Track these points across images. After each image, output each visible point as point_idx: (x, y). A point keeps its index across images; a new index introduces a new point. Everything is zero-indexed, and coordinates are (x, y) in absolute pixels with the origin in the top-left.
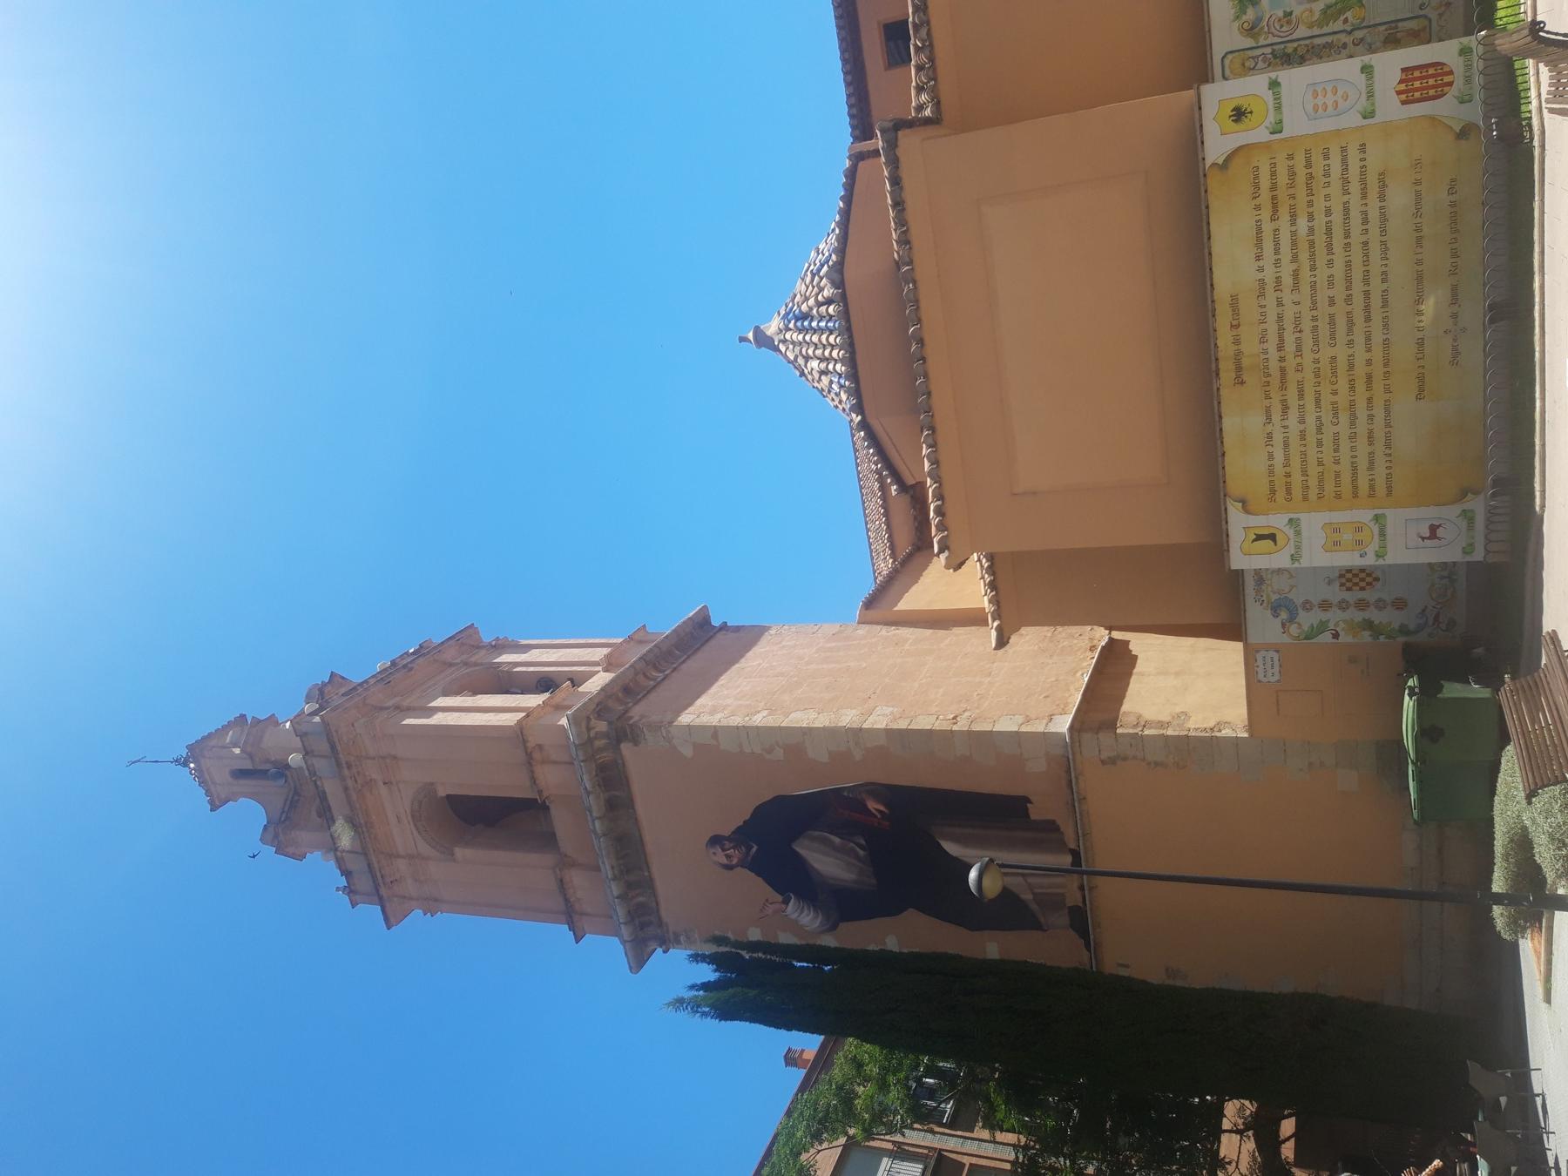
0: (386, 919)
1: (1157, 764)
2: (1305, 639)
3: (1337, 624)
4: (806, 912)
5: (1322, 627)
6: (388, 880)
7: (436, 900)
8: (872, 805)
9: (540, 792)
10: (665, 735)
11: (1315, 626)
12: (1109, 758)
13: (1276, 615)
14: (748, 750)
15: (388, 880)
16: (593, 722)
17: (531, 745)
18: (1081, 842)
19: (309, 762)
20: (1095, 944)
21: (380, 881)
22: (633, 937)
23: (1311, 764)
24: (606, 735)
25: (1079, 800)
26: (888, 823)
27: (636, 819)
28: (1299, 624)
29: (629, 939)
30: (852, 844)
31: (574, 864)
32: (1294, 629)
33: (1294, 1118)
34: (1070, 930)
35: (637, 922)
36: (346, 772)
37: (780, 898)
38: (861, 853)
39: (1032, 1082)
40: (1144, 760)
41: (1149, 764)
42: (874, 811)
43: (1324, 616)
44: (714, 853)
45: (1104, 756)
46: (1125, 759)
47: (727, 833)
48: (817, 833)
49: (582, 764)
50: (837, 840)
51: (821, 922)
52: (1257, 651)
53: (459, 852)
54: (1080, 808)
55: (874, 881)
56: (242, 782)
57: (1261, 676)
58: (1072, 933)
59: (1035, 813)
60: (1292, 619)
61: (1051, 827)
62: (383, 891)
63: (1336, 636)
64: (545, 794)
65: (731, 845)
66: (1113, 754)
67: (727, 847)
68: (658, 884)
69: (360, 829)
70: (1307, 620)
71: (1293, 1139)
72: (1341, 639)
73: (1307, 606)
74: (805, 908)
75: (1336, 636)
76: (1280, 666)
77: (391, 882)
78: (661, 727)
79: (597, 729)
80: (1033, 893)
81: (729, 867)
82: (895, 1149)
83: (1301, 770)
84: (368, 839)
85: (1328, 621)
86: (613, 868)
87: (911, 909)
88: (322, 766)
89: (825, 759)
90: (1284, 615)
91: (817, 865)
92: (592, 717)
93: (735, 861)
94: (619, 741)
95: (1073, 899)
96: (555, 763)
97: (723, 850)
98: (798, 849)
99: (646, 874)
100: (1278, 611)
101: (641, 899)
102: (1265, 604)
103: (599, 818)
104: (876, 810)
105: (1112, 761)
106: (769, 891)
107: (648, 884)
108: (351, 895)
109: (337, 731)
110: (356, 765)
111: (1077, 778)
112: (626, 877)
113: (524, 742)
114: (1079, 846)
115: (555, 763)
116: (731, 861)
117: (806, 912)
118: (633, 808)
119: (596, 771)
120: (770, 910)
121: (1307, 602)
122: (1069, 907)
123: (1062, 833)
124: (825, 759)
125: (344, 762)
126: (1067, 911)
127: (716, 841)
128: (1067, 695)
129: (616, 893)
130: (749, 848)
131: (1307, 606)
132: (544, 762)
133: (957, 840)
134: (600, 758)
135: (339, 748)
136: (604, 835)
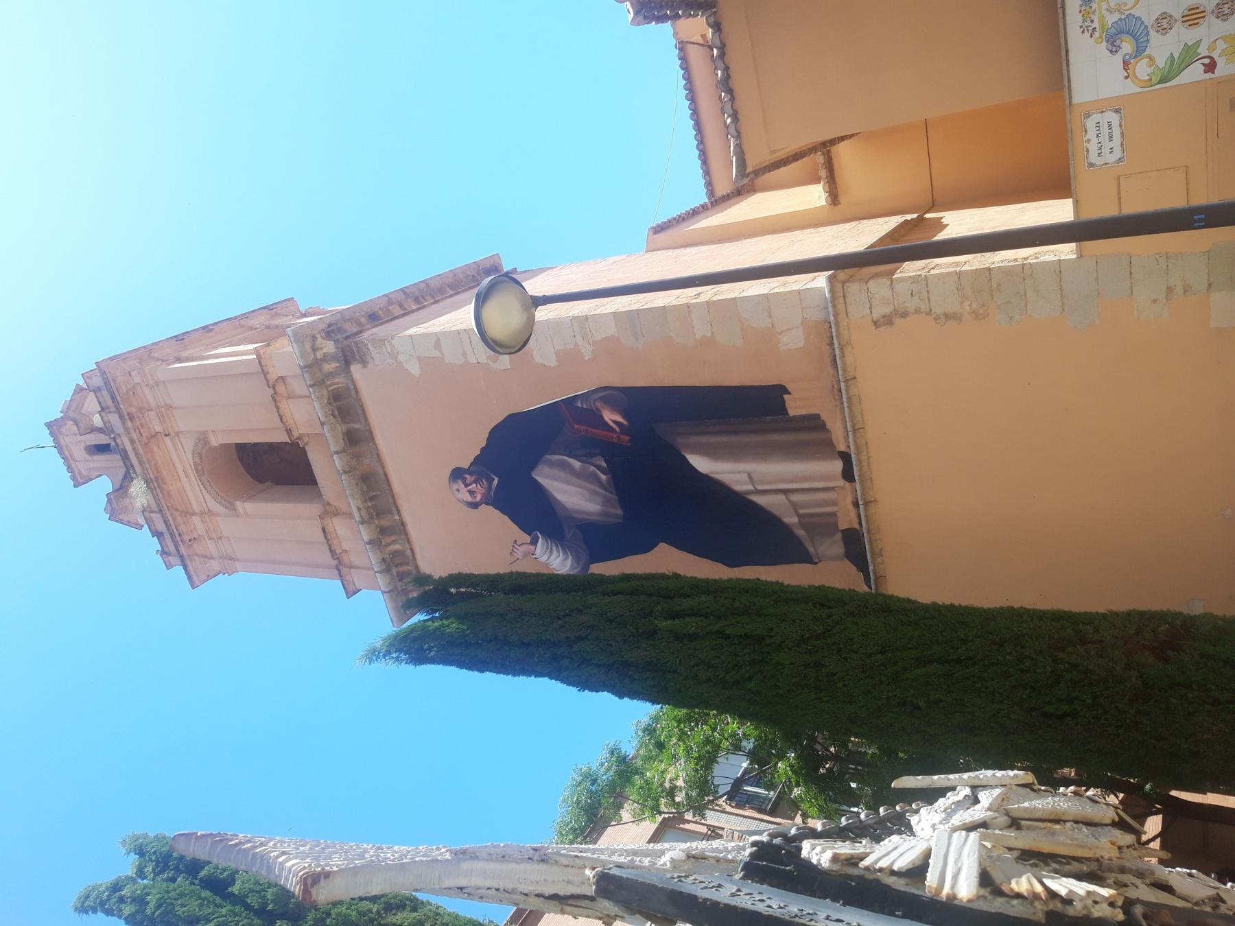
0: (190, 577)
1: (947, 316)
2: (1160, 82)
3: (1213, 46)
4: (555, 553)
5: (1189, 55)
6: (186, 538)
7: (231, 559)
8: (610, 416)
9: (289, 431)
10: (389, 350)
11: (1176, 56)
12: (884, 317)
13: (1114, 49)
14: (472, 360)
15: (186, 538)
16: (320, 341)
17: (272, 376)
18: (851, 439)
19: (105, 418)
20: (876, 579)
21: (178, 538)
22: (391, 587)
23: (1170, 290)
24: (334, 358)
25: (846, 381)
26: (627, 438)
27: (378, 455)
28: (1151, 58)
29: (387, 590)
30: (592, 468)
31: (337, 513)
32: (1142, 69)
33: (1161, 816)
34: (845, 559)
35: (394, 571)
36: (129, 424)
37: (528, 539)
38: (603, 477)
39: (437, 615)
40: (929, 313)
41: (937, 318)
42: (611, 424)
43: (1190, 35)
44: (458, 490)
45: (879, 312)
46: (904, 315)
47: (466, 465)
48: (556, 457)
49: (311, 389)
50: (577, 464)
51: (572, 565)
52: (1088, 116)
53: (243, 506)
54: (847, 391)
55: (620, 512)
56: (96, 457)
57: (1093, 158)
58: (847, 562)
59: (795, 407)
60: (1139, 51)
61: (813, 423)
62: (183, 549)
63: (1211, 67)
64: (295, 434)
65: (473, 479)
66: (887, 310)
67: (468, 481)
68: (411, 528)
69: (151, 485)
70: (1163, 48)
71: (1159, 840)
72: (1220, 71)
73: (1164, 23)
74: (554, 548)
75: (1211, 67)
76: (1122, 134)
77: (190, 540)
78: (384, 340)
79: (325, 350)
80: (799, 516)
81: (474, 505)
82: (709, 832)
83: (1155, 301)
84: (160, 495)
85: (1198, 44)
86: (359, 509)
87: (662, 544)
88: (114, 419)
89: (553, 363)
90: (1127, 47)
91: (560, 497)
92: (318, 336)
93: (479, 498)
94: (347, 363)
95: (847, 519)
96: (300, 397)
97: (467, 486)
98: (539, 479)
99: (397, 517)
100: (1117, 43)
101: (397, 547)
102: (1097, 35)
103: (337, 453)
104: (615, 422)
105: (888, 320)
106: (514, 531)
107: (400, 530)
108: (164, 556)
109: (114, 381)
110: (138, 417)
111: (842, 349)
112: (377, 522)
113: (265, 373)
114: (849, 447)
115: (300, 397)
116: (475, 497)
117: (555, 553)
118: (374, 443)
119: (329, 399)
120: (520, 551)
121: (1164, 16)
122: (843, 531)
123: (828, 431)
124: (553, 363)
125: (125, 414)
126: (839, 536)
127: (457, 474)
128: (1080, 709)
129: (366, 538)
130: (490, 481)
131: (1164, 23)
132: (291, 396)
133: (711, 452)
134: (331, 385)
135: (118, 398)
136: (345, 472)
